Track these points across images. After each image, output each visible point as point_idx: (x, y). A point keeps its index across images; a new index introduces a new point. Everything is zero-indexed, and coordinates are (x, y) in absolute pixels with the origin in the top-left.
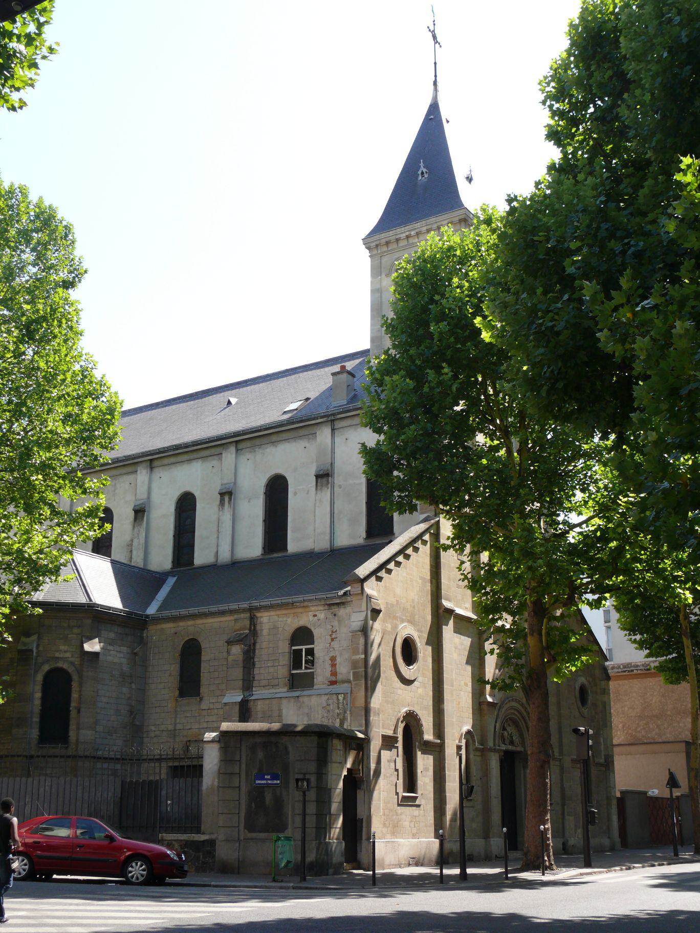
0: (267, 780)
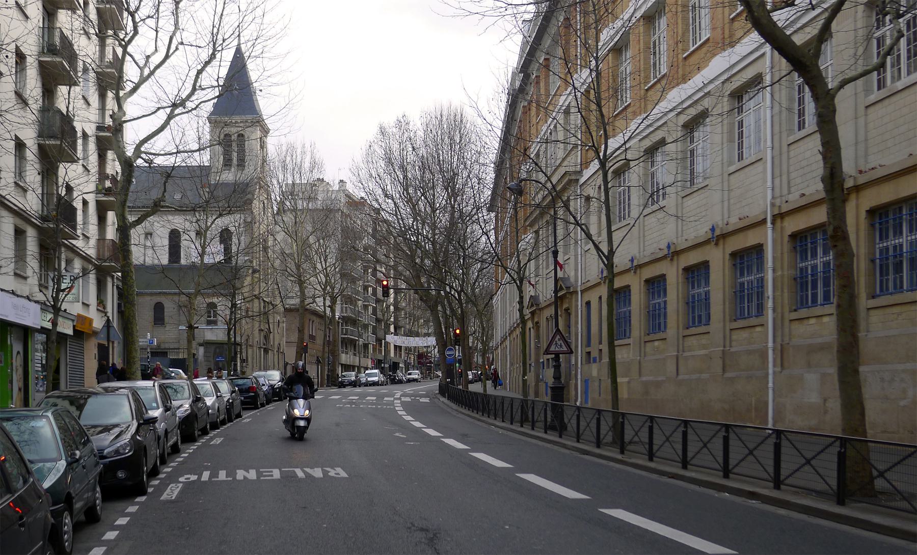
0: (220, 359)
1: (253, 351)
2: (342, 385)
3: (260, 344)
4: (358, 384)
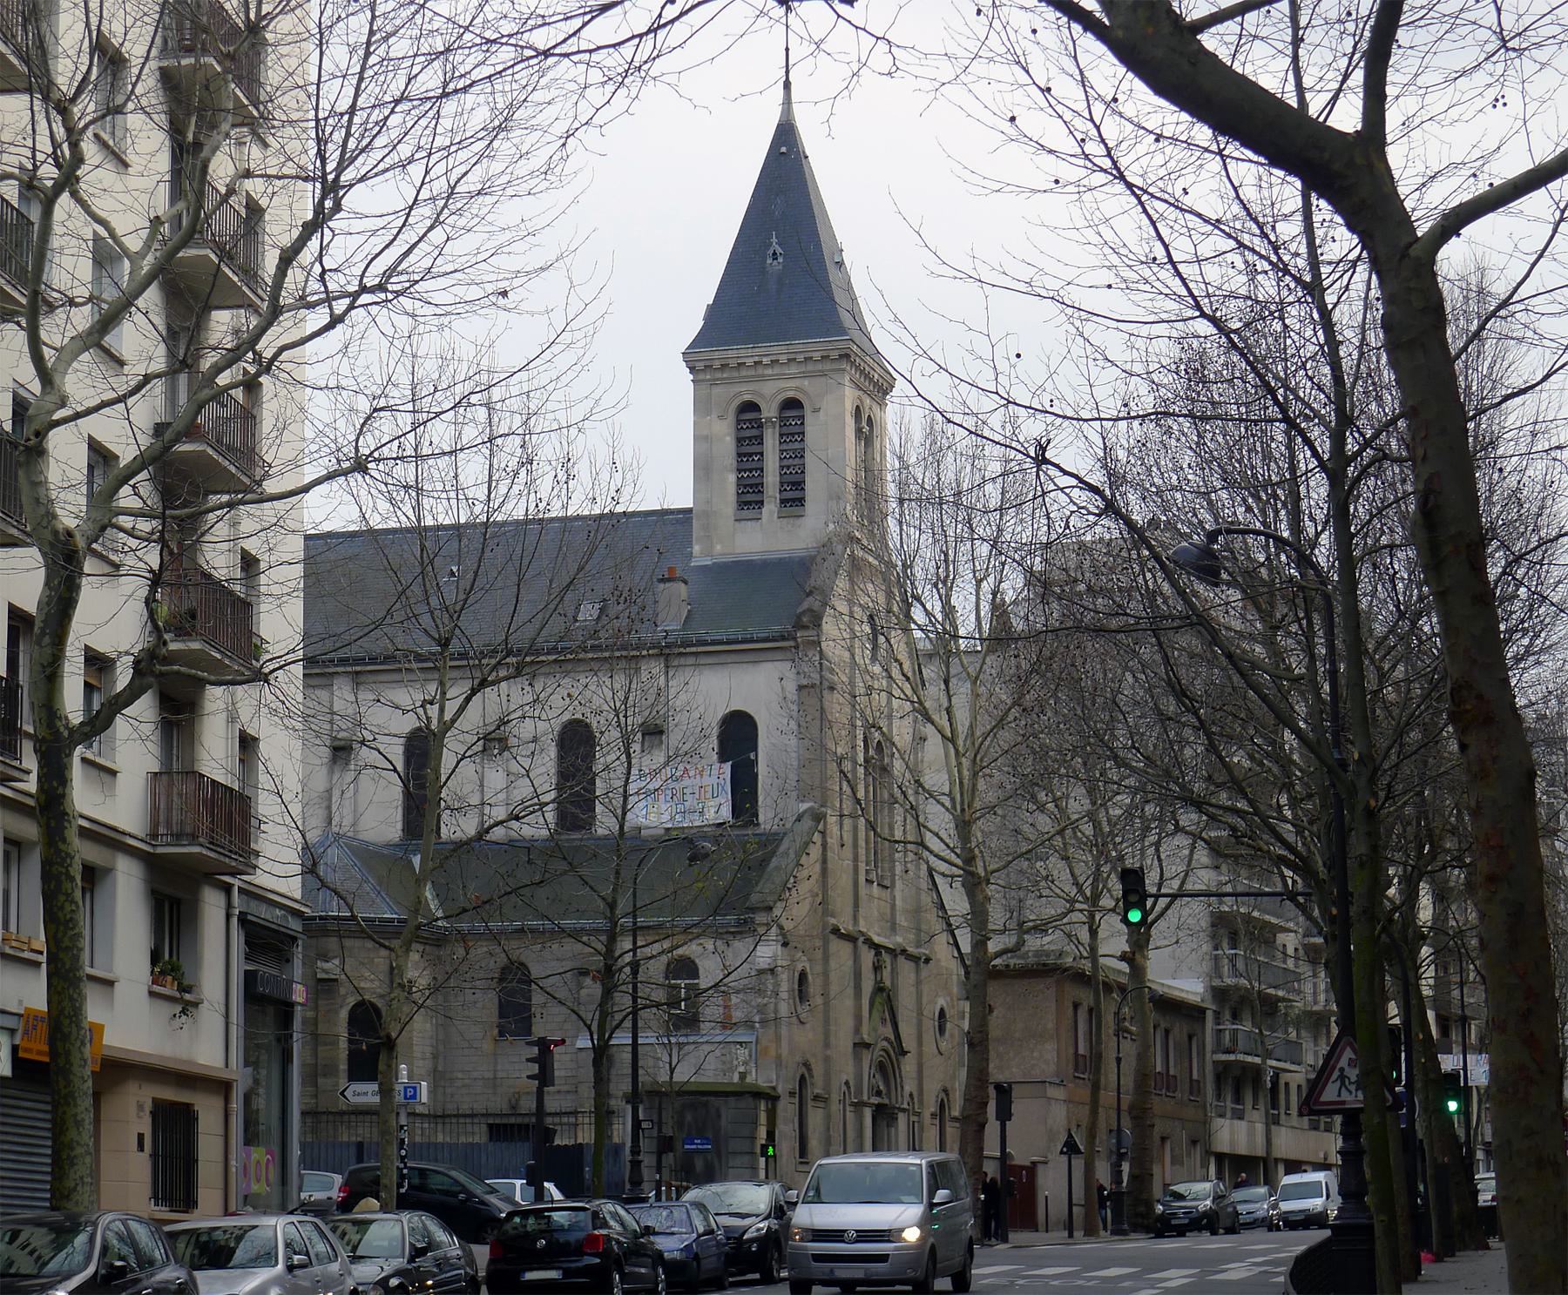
0: (697, 1145)
1: (828, 1117)
2: (1164, 1227)
3: (859, 1091)
4: (1225, 1222)
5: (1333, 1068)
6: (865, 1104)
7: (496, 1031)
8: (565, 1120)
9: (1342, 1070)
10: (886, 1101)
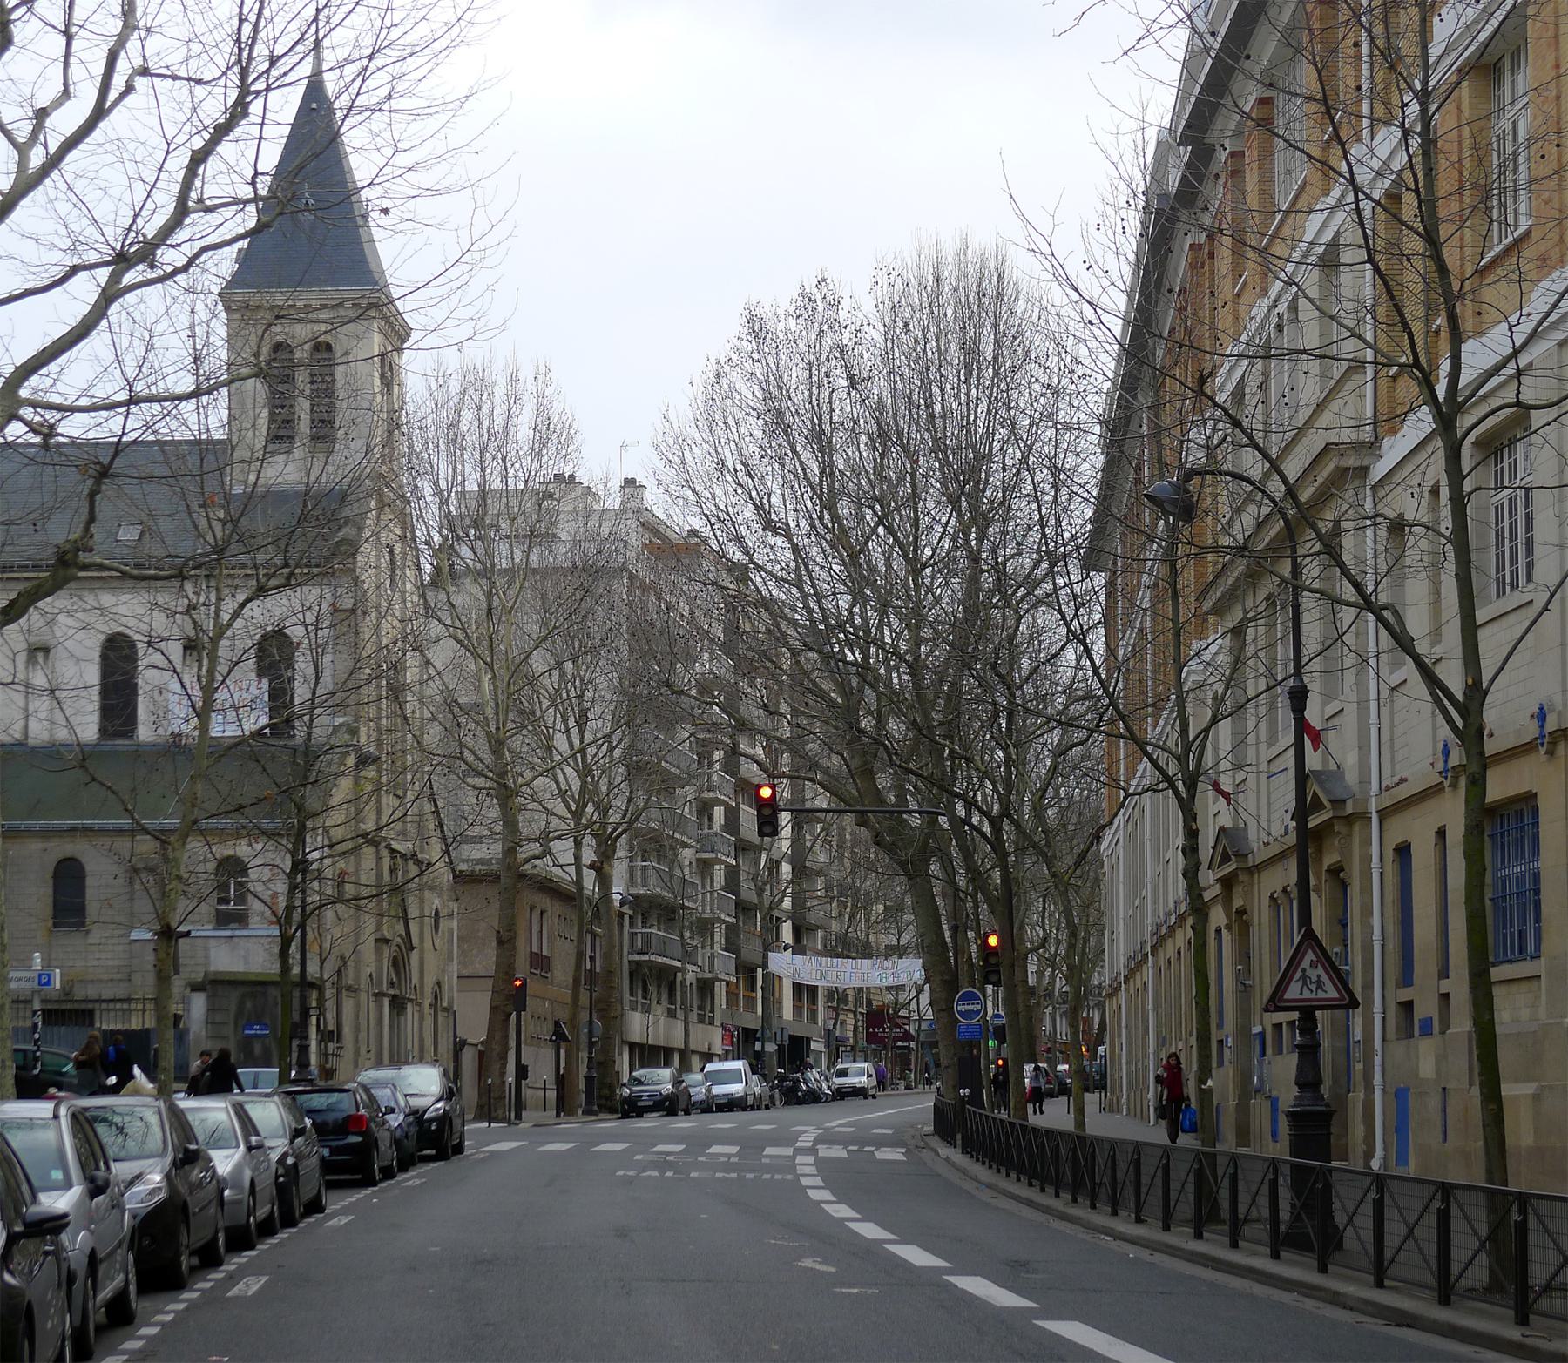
0: (256, 1030)
1: (358, 1006)
2: (632, 1109)
3: (380, 983)
5: (1296, 969)
6: (384, 995)
7: (50, 923)
8: (118, 1006)
9: (1304, 970)
10: (397, 992)
